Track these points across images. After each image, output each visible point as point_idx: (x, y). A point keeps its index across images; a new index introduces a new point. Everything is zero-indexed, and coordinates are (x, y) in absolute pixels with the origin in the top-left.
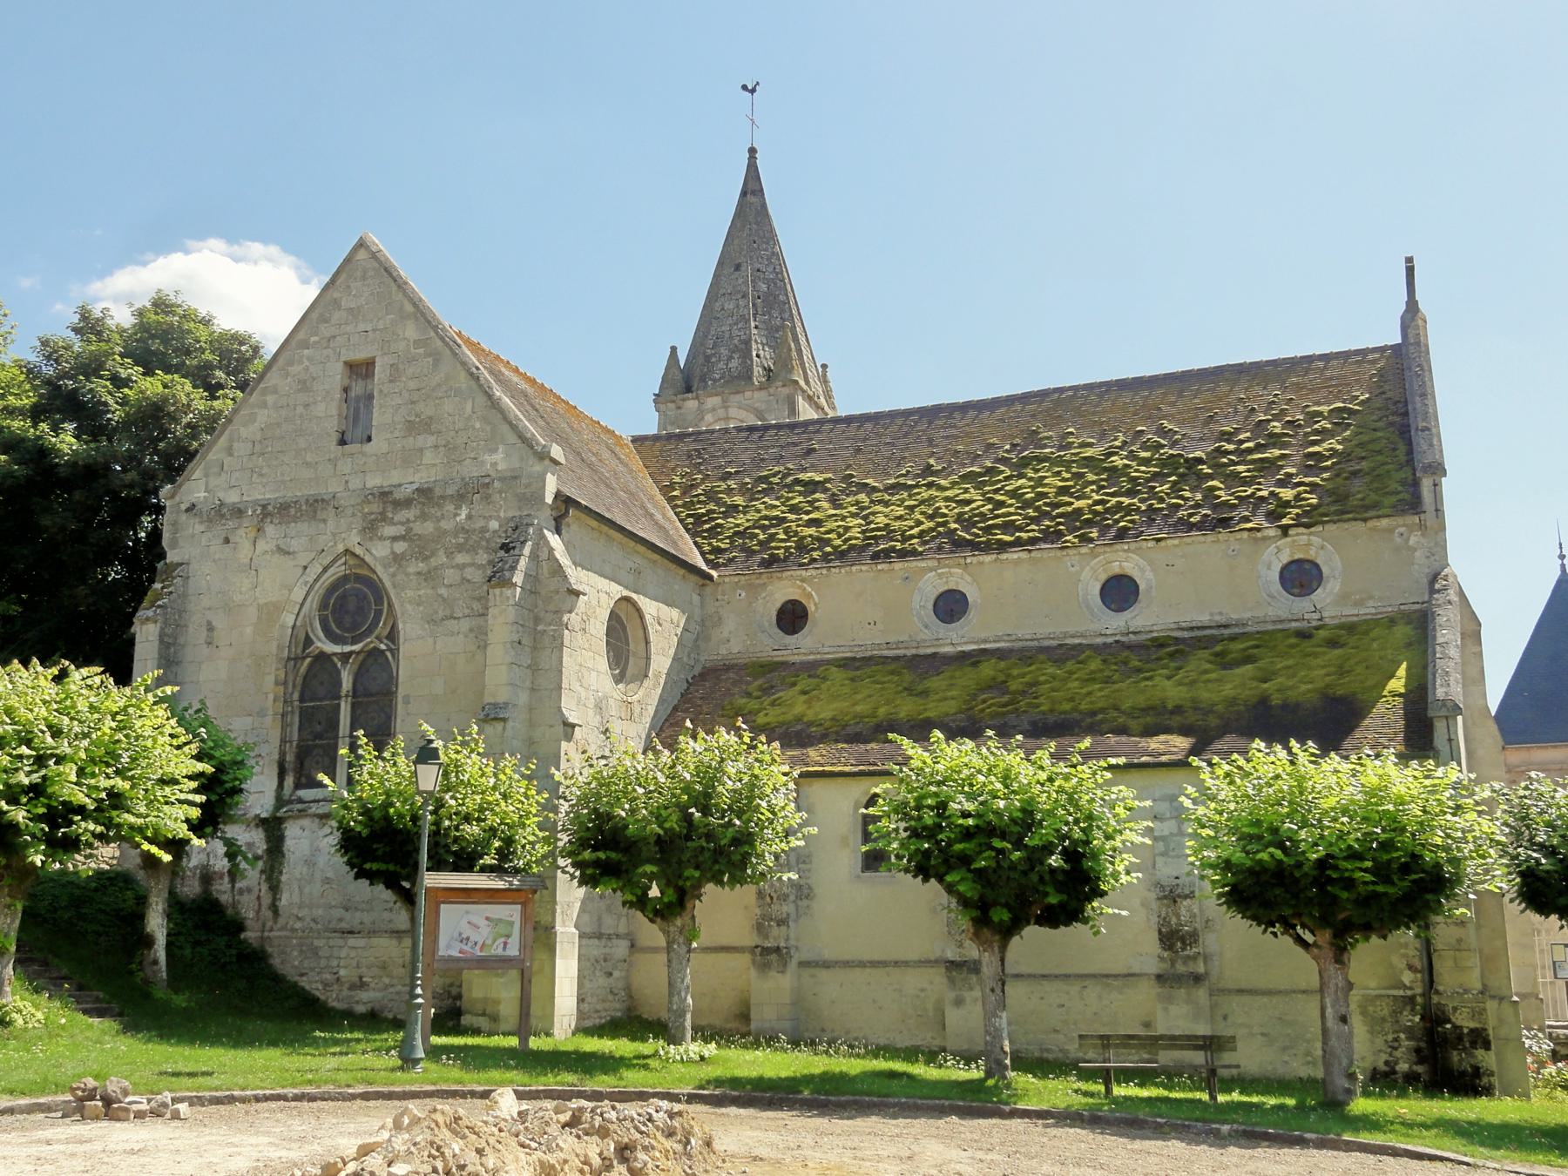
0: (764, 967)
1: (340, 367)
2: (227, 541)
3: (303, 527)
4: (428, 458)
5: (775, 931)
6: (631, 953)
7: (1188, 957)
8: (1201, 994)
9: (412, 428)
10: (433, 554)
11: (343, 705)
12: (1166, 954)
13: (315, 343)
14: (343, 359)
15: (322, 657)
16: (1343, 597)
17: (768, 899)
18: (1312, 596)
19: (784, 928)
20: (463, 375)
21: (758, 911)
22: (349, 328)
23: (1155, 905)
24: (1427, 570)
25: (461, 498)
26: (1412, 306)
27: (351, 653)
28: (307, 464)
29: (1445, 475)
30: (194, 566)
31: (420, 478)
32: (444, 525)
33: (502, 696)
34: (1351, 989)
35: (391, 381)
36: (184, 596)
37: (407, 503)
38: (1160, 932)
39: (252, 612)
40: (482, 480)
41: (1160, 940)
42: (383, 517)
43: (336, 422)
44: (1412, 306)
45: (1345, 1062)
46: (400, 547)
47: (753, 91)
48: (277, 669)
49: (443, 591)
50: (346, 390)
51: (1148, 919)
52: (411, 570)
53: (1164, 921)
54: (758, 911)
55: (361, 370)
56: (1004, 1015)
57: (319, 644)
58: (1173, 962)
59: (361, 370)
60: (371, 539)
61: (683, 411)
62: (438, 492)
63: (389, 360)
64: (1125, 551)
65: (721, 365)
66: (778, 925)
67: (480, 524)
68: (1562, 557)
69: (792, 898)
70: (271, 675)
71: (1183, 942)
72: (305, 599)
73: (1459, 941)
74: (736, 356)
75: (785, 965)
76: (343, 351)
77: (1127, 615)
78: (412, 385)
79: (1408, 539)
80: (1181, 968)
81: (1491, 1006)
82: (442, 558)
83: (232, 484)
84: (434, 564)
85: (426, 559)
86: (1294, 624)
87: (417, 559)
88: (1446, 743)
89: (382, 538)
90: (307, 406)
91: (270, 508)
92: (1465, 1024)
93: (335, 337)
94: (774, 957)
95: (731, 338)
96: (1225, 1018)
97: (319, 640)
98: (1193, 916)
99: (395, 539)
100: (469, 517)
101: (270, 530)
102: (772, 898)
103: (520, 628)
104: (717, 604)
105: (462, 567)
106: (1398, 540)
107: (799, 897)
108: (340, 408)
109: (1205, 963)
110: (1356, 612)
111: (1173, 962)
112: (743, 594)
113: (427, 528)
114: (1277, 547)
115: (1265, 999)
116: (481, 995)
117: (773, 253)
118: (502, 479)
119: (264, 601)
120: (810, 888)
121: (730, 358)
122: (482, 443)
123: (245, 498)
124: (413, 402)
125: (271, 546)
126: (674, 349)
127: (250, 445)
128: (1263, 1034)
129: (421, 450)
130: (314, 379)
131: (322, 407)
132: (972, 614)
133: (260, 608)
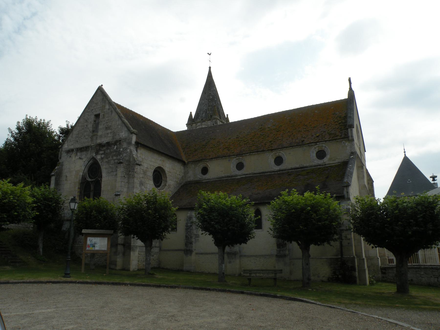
2: (70, 157)
3: (85, 153)
4: (109, 135)
6: (160, 251)
9: (107, 128)
10: (109, 157)
11: (91, 193)
12: (278, 249)
14: (94, 114)
15: (88, 182)
16: (330, 159)
20: (117, 116)
24: (350, 151)
26: (351, 89)
27: (93, 181)
28: (86, 139)
32: (112, 150)
41: (277, 246)
44: (351, 89)
46: (103, 156)
47: (210, 54)
48: (78, 185)
49: (111, 166)
50: (95, 121)
55: (97, 116)
56: (223, 265)
57: (87, 179)
59: (97, 116)
61: (192, 126)
63: (103, 113)
64: (279, 151)
68: (405, 152)
69: (194, 237)
70: (77, 186)
74: (204, 113)
76: (94, 113)
77: (280, 166)
78: (107, 119)
79: (345, 144)
82: (111, 158)
84: (109, 159)
85: (107, 158)
88: (346, 193)
89: (99, 154)
93: (93, 110)
95: (203, 109)
99: (102, 154)
100: (117, 148)
101: (79, 154)
102: (189, 238)
104: (188, 169)
105: (114, 160)
106: (343, 144)
110: (333, 162)
112: (193, 166)
114: (315, 148)
117: (214, 90)
121: (203, 114)
122: (120, 131)
124: (107, 123)
125: (78, 158)
126: (191, 113)
129: (108, 134)
132: (245, 168)
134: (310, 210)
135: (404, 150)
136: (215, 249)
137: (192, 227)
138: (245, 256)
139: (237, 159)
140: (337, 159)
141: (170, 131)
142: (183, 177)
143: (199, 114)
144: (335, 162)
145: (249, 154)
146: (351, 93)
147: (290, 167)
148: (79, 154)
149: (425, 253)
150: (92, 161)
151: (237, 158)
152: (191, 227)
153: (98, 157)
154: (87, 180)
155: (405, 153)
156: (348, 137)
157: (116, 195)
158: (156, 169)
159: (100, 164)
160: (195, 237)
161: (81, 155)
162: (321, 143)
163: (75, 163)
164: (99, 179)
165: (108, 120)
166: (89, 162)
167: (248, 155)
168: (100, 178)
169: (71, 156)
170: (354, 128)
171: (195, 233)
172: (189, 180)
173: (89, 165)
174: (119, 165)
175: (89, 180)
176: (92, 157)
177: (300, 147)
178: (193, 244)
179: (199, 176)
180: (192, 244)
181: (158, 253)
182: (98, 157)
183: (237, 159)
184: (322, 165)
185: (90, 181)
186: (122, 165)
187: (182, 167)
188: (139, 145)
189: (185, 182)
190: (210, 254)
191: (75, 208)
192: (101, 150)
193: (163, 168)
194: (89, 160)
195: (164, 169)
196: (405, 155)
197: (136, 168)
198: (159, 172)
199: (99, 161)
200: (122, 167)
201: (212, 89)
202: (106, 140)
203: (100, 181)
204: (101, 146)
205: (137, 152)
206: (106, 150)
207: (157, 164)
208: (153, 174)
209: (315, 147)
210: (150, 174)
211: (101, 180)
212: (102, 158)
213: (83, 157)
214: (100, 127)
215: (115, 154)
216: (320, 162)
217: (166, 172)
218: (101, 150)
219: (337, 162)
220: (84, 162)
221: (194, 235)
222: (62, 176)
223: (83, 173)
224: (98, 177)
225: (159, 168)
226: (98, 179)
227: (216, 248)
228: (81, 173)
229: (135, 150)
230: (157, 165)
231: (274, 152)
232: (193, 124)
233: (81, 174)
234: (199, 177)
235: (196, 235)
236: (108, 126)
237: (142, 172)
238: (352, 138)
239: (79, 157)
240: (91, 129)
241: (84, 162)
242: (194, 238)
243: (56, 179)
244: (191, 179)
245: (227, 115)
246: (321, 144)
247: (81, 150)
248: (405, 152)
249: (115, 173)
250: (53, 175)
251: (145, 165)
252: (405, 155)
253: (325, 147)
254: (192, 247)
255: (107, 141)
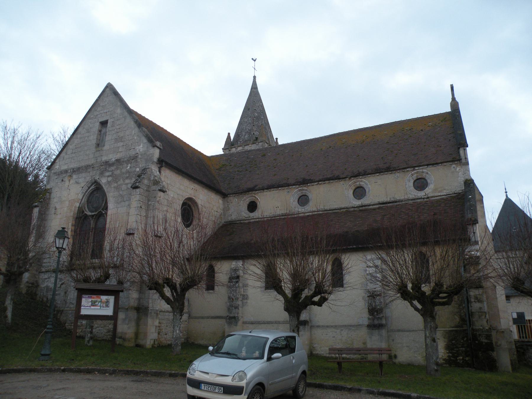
0: (230, 323)
1: (98, 124)
2: (62, 180)
5: (234, 311)
6: (189, 318)
7: (379, 318)
8: (384, 332)
9: (117, 140)
10: (119, 180)
12: (371, 317)
13: (92, 117)
14: (100, 121)
15: (86, 216)
16: (435, 190)
17: (232, 299)
18: (424, 191)
19: (237, 310)
21: (228, 304)
22: (102, 112)
23: (367, 299)
24: (463, 179)
25: (128, 161)
26: (454, 99)
27: (94, 215)
29: (467, 146)
30: (54, 191)
31: (118, 156)
33: (134, 225)
34: (437, 328)
35: (112, 127)
36: (50, 199)
37: (112, 164)
38: (368, 309)
39: (67, 203)
40: (135, 155)
41: (369, 312)
42: (106, 170)
43: (95, 141)
44: (454, 99)
45: (435, 358)
47: (255, 61)
48: (72, 221)
49: (121, 193)
50: (100, 131)
51: (365, 305)
52: (112, 186)
53: (370, 305)
54: (228, 304)
55: (104, 124)
57: (86, 212)
58: (373, 320)
59: (104, 124)
60: (102, 177)
62: (122, 160)
63: (112, 120)
64: (361, 178)
65: (243, 137)
66: (235, 309)
67: (134, 169)
68: (506, 192)
69: (240, 299)
71: (377, 312)
72: (82, 199)
73: (481, 308)
74: (247, 134)
75: (237, 323)
78: (118, 127)
80: (376, 322)
81: (494, 333)
82: (121, 182)
83: (66, 163)
84: (119, 184)
85: (117, 182)
86: (419, 200)
87: (114, 182)
89: (105, 177)
90: (88, 137)
91: (75, 169)
92: (484, 341)
94: (233, 320)
96: (393, 340)
97: (86, 211)
98: (381, 302)
99: (108, 176)
100: (130, 167)
102: (233, 299)
103: (141, 203)
104: (228, 203)
105: (127, 184)
106: (453, 169)
107: (243, 299)
108: (97, 137)
109: (386, 320)
110: (439, 194)
111: (373, 320)
112: (236, 200)
113: (118, 172)
115: (408, 333)
116: (121, 331)
117: (260, 105)
118: (141, 155)
119: (71, 199)
120: (247, 296)
121: (245, 135)
122: (136, 143)
123: (69, 167)
126: (229, 134)
127: (72, 150)
128: (407, 346)
129: (119, 147)
130: (91, 128)
131: (92, 137)
132: (311, 203)
133: (69, 201)
134: (299, 285)
135: (506, 190)
136: (285, 315)
137: (239, 284)
138: (318, 326)
139: (300, 190)
140: (445, 189)
141: (202, 154)
142: (221, 215)
143: (240, 136)
144: (442, 194)
145: (317, 183)
146: (455, 104)
147: (377, 200)
148: (75, 176)
149: (530, 326)
150: (95, 186)
151: (299, 189)
152: (237, 285)
153: (103, 181)
154: (85, 214)
155: (507, 194)
156: (460, 160)
157: (129, 234)
158: (185, 201)
159: (106, 191)
160: (241, 299)
161: (78, 178)
162: (421, 168)
163: (69, 190)
164: (104, 212)
165: (119, 128)
166: (89, 188)
167: (316, 185)
168: (105, 211)
169: (63, 179)
170: (467, 148)
171: (242, 293)
172: (230, 219)
173: (89, 192)
174: (134, 190)
175: (89, 213)
176: (93, 181)
177: (391, 173)
178: (240, 308)
179: (245, 214)
180: (238, 309)
181: (186, 321)
182: (103, 181)
183: (300, 190)
184: (424, 199)
185: (90, 216)
186: (138, 190)
187: (221, 201)
188: (164, 164)
189: (224, 222)
190: (265, 323)
191: (64, 247)
192: (108, 170)
193: (196, 200)
194: (89, 186)
195: (197, 201)
196: (507, 195)
197: (159, 196)
198: (189, 206)
199: (104, 187)
200: (138, 193)
201: (258, 104)
202: (115, 157)
203: (105, 215)
204: (107, 163)
205: (160, 174)
206: (115, 170)
207: (188, 194)
208: (182, 208)
209: (412, 173)
210: (178, 207)
211: (106, 213)
212: (109, 183)
213: (81, 180)
214: (108, 138)
215: (128, 175)
216: (421, 194)
217: (200, 206)
218: (109, 171)
219: (445, 194)
220: (83, 187)
221: (240, 295)
222: (49, 208)
223: (80, 203)
224: (102, 209)
225: (190, 199)
226: (102, 213)
227: (286, 314)
228: (77, 203)
229: (158, 171)
230: (187, 196)
231: (353, 181)
232: (231, 148)
233: (78, 205)
234: (245, 215)
235: (244, 295)
236: (119, 137)
237: (166, 203)
238: (466, 160)
239: (76, 181)
240: (94, 142)
241: (83, 187)
242: (241, 301)
243: (40, 212)
244: (233, 218)
245: (277, 139)
246: (421, 169)
247: (77, 171)
248: (506, 192)
249: (127, 203)
250: (36, 206)
251: (171, 194)
252: (507, 195)
253: (427, 173)
254: (238, 314)
255: (116, 158)
